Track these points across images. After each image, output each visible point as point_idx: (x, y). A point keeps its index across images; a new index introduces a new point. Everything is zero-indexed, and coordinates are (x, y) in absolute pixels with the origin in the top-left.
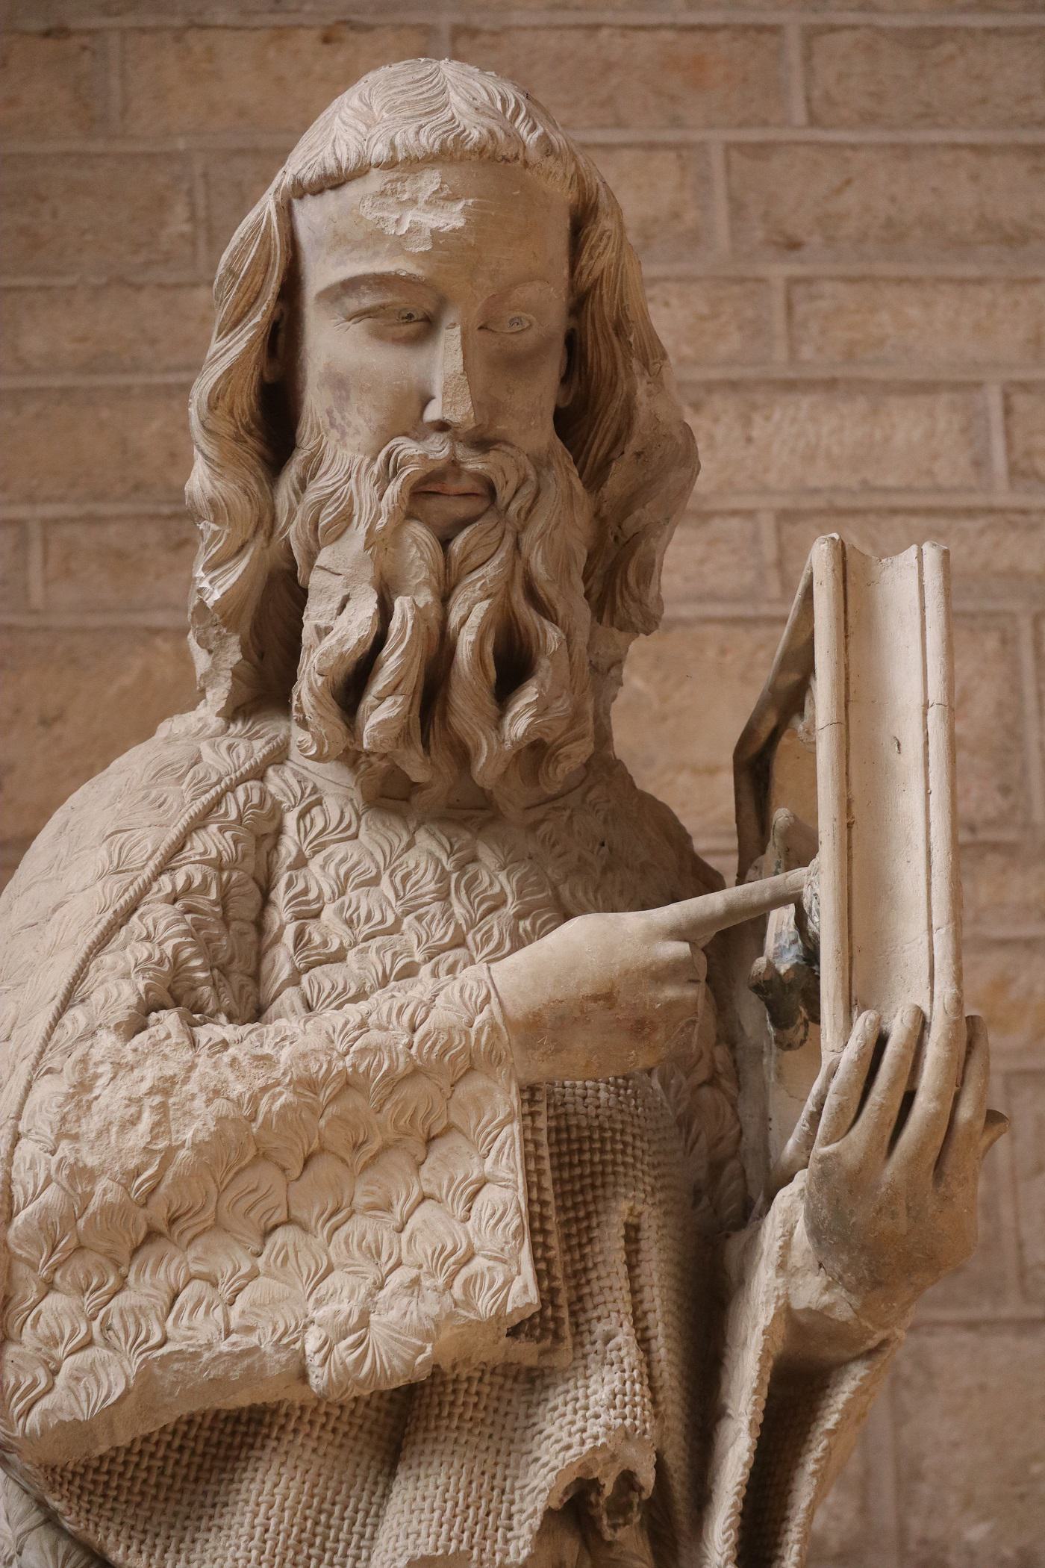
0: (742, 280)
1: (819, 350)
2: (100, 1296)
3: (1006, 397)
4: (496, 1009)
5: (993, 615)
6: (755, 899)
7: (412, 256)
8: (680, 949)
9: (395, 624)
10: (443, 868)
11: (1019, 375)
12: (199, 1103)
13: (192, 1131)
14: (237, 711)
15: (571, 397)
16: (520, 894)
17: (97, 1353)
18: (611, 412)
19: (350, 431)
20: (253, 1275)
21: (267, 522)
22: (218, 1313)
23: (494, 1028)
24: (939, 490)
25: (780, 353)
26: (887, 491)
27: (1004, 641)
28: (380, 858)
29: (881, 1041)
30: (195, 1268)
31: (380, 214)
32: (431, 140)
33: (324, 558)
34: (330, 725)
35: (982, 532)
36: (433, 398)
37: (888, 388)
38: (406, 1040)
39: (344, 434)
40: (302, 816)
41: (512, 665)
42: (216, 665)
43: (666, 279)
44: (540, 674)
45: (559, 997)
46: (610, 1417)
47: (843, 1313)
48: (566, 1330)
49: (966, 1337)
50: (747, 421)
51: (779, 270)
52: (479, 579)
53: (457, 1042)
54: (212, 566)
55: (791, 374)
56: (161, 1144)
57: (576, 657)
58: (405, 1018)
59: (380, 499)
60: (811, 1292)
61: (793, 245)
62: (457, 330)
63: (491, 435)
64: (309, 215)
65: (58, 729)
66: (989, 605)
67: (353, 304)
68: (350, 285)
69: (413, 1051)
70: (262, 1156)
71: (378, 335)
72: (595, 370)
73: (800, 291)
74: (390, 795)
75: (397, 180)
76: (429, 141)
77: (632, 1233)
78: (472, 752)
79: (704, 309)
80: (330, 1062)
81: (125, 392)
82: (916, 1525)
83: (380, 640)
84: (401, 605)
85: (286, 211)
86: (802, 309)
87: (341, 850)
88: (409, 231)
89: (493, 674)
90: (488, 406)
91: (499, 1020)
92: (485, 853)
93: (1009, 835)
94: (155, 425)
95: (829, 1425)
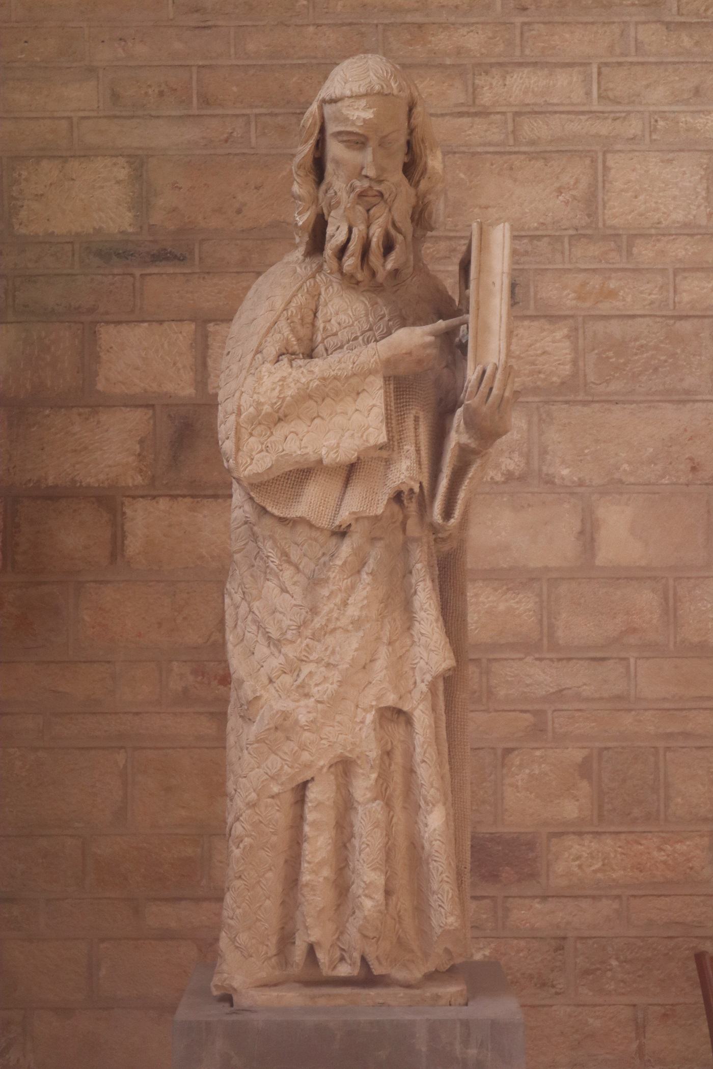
0: (505, 23)
1: (532, 51)
2: (265, 438)
3: (599, 68)
5: (589, 151)
6: (454, 324)
7: (358, 127)
8: (430, 339)
9: (353, 236)
11: (604, 60)
12: (292, 385)
13: (290, 392)
16: (390, 314)
17: (264, 453)
20: (308, 432)
21: (316, 200)
22: (298, 443)
24: (572, 104)
25: (518, 53)
26: (553, 104)
27: (592, 161)
29: (484, 372)
30: (293, 430)
33: (332, 214)
34: (334, 264)
35: (587, 120)
37: (556, 65)
40: (326, 290)
41: (388, 247)
42: (302, 240)
43: (477, 23)
46: (407, 474)
47: (473, 445)
48: (396, 448)
49: (566, 406)
50: (504, 79)
51: (519, 20)
54: (299, 214)
55: (521, 60)
56: (282, 396)
60: (465, 439)
61: (525, 9)
63: (381, 179)
64: (328, 109)
65: (260, 191)
66: (588, 148)
68: (340, 133)
70: (310, 397)
71: (348, 147)
73: (526, 27)
74: (350, 282)
76: (363, 90)
77: (416, 419)
79: (490, 35)
81: (283, 66)
82: (545, 468)
83: (348, 240)
84: (355, 230)
85: (321, 108)
86: (527, 34)
89: (382, 250)
90: (381, 169)
92: (379, 300)
93: (589, 232)
94: (294, 79)
95: (470, 475)
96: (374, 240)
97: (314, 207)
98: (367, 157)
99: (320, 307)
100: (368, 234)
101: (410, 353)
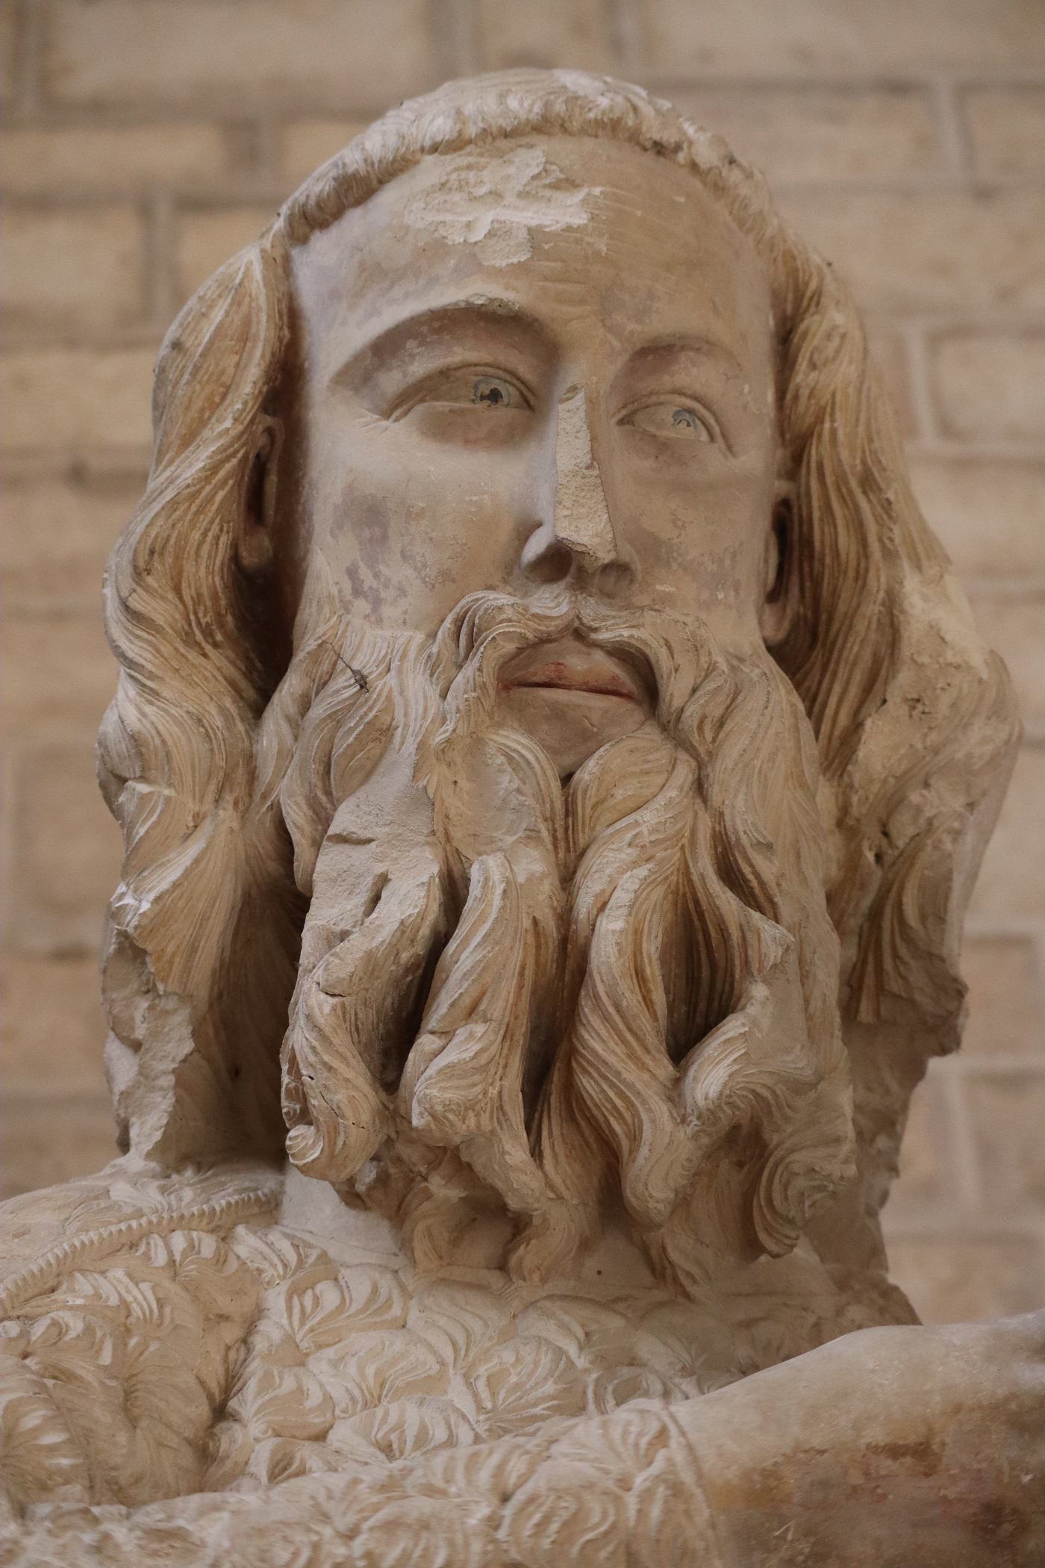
4: (680, 1456)
10: (571, 1364)
14: (182, 1153)
15: (786, 625)
18: (860, 626)
19: (386, 594)
23: (677, 1490)
28: (448, 1353)
31: (440, 218)
32: (526, 104)
36: (539, 525)
38: (484, 1510)
39: (377, 602)
41: (700, 991)
44: (752, 1010)
45: (817, 1442)
52: (628, 827)
53: (595, 1519)
57: (816, 1004)
58: (484, 1476)
59: (444, 696)
62: (579, 400)
67: (392, 381)
68: (386, 348)
69: (502, 1534)
71: (440, 430)
72: (828, 560)
75: (469, 167)
78: (625, 1143)
80: (316, 1547)
87: (363, 1341)
88: (490, 234)
91: (688, 1477)
96: (611, 928)
97: (228, 816)
98: (558, 478)
99: (255, 1367)
100: (565, 916)
101: (920, 1453)
